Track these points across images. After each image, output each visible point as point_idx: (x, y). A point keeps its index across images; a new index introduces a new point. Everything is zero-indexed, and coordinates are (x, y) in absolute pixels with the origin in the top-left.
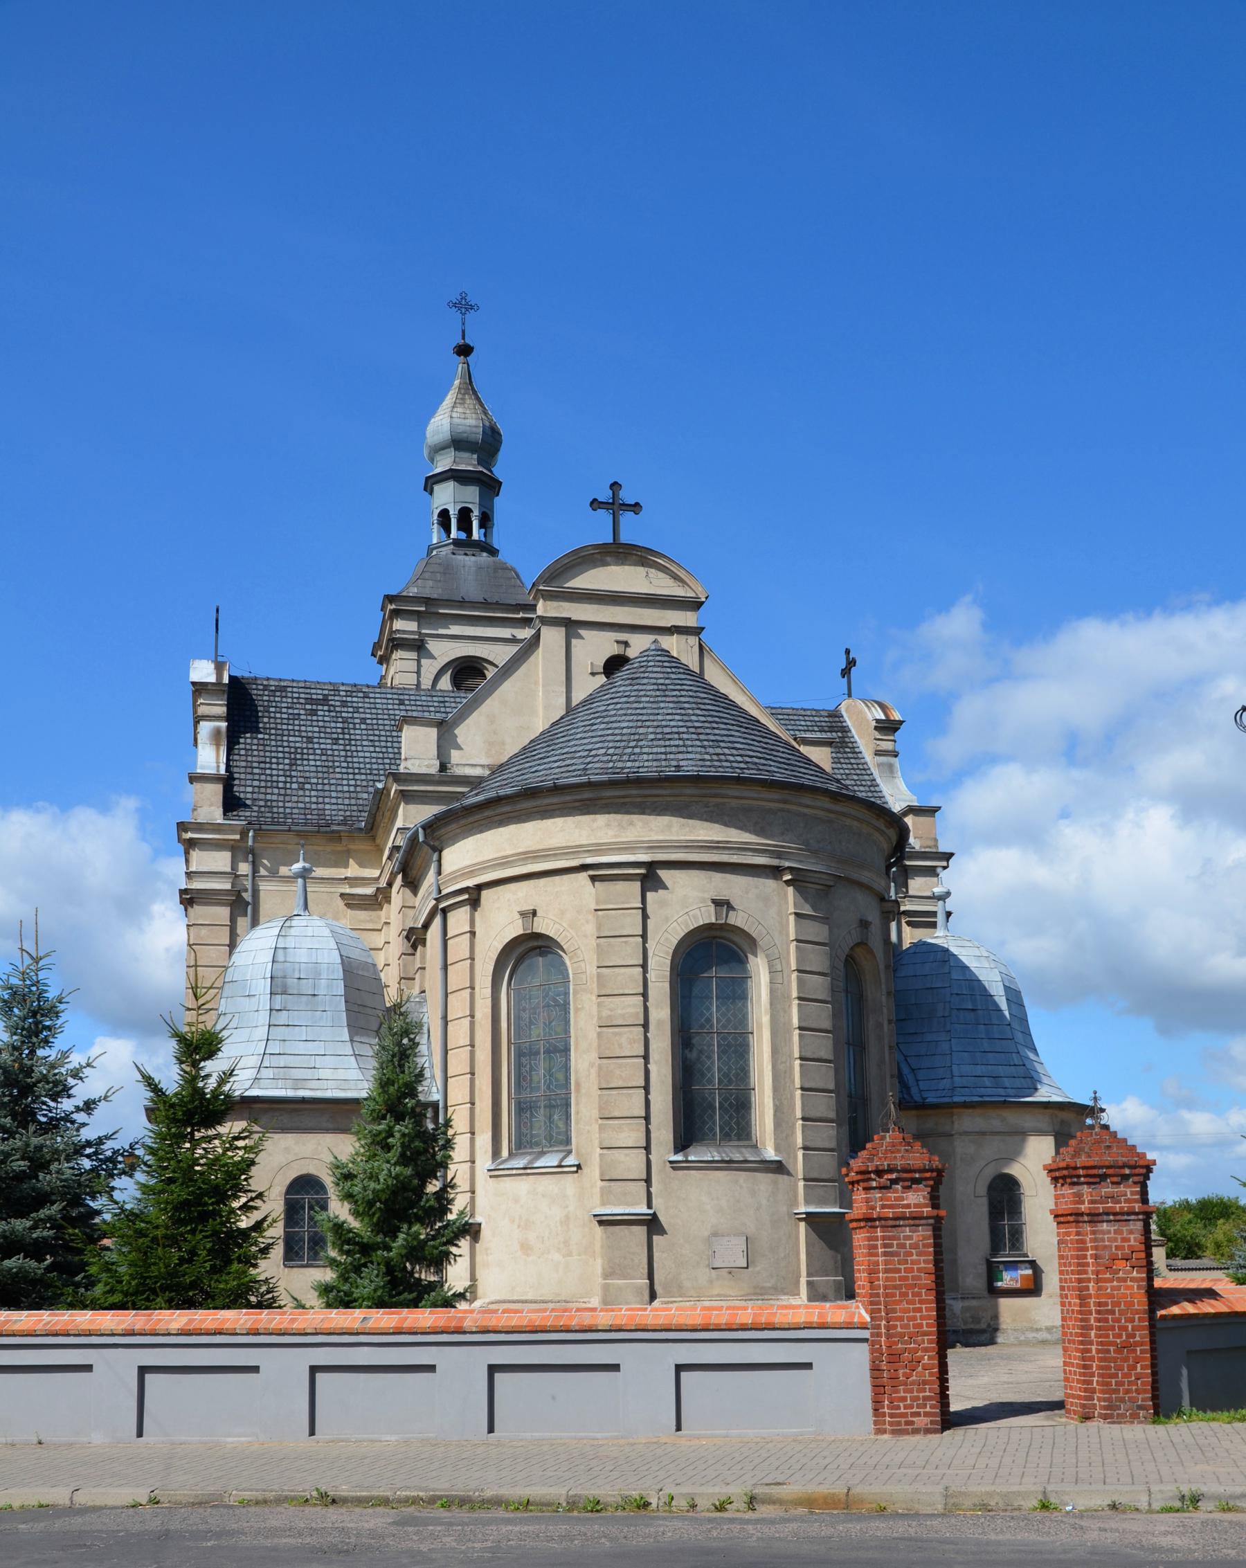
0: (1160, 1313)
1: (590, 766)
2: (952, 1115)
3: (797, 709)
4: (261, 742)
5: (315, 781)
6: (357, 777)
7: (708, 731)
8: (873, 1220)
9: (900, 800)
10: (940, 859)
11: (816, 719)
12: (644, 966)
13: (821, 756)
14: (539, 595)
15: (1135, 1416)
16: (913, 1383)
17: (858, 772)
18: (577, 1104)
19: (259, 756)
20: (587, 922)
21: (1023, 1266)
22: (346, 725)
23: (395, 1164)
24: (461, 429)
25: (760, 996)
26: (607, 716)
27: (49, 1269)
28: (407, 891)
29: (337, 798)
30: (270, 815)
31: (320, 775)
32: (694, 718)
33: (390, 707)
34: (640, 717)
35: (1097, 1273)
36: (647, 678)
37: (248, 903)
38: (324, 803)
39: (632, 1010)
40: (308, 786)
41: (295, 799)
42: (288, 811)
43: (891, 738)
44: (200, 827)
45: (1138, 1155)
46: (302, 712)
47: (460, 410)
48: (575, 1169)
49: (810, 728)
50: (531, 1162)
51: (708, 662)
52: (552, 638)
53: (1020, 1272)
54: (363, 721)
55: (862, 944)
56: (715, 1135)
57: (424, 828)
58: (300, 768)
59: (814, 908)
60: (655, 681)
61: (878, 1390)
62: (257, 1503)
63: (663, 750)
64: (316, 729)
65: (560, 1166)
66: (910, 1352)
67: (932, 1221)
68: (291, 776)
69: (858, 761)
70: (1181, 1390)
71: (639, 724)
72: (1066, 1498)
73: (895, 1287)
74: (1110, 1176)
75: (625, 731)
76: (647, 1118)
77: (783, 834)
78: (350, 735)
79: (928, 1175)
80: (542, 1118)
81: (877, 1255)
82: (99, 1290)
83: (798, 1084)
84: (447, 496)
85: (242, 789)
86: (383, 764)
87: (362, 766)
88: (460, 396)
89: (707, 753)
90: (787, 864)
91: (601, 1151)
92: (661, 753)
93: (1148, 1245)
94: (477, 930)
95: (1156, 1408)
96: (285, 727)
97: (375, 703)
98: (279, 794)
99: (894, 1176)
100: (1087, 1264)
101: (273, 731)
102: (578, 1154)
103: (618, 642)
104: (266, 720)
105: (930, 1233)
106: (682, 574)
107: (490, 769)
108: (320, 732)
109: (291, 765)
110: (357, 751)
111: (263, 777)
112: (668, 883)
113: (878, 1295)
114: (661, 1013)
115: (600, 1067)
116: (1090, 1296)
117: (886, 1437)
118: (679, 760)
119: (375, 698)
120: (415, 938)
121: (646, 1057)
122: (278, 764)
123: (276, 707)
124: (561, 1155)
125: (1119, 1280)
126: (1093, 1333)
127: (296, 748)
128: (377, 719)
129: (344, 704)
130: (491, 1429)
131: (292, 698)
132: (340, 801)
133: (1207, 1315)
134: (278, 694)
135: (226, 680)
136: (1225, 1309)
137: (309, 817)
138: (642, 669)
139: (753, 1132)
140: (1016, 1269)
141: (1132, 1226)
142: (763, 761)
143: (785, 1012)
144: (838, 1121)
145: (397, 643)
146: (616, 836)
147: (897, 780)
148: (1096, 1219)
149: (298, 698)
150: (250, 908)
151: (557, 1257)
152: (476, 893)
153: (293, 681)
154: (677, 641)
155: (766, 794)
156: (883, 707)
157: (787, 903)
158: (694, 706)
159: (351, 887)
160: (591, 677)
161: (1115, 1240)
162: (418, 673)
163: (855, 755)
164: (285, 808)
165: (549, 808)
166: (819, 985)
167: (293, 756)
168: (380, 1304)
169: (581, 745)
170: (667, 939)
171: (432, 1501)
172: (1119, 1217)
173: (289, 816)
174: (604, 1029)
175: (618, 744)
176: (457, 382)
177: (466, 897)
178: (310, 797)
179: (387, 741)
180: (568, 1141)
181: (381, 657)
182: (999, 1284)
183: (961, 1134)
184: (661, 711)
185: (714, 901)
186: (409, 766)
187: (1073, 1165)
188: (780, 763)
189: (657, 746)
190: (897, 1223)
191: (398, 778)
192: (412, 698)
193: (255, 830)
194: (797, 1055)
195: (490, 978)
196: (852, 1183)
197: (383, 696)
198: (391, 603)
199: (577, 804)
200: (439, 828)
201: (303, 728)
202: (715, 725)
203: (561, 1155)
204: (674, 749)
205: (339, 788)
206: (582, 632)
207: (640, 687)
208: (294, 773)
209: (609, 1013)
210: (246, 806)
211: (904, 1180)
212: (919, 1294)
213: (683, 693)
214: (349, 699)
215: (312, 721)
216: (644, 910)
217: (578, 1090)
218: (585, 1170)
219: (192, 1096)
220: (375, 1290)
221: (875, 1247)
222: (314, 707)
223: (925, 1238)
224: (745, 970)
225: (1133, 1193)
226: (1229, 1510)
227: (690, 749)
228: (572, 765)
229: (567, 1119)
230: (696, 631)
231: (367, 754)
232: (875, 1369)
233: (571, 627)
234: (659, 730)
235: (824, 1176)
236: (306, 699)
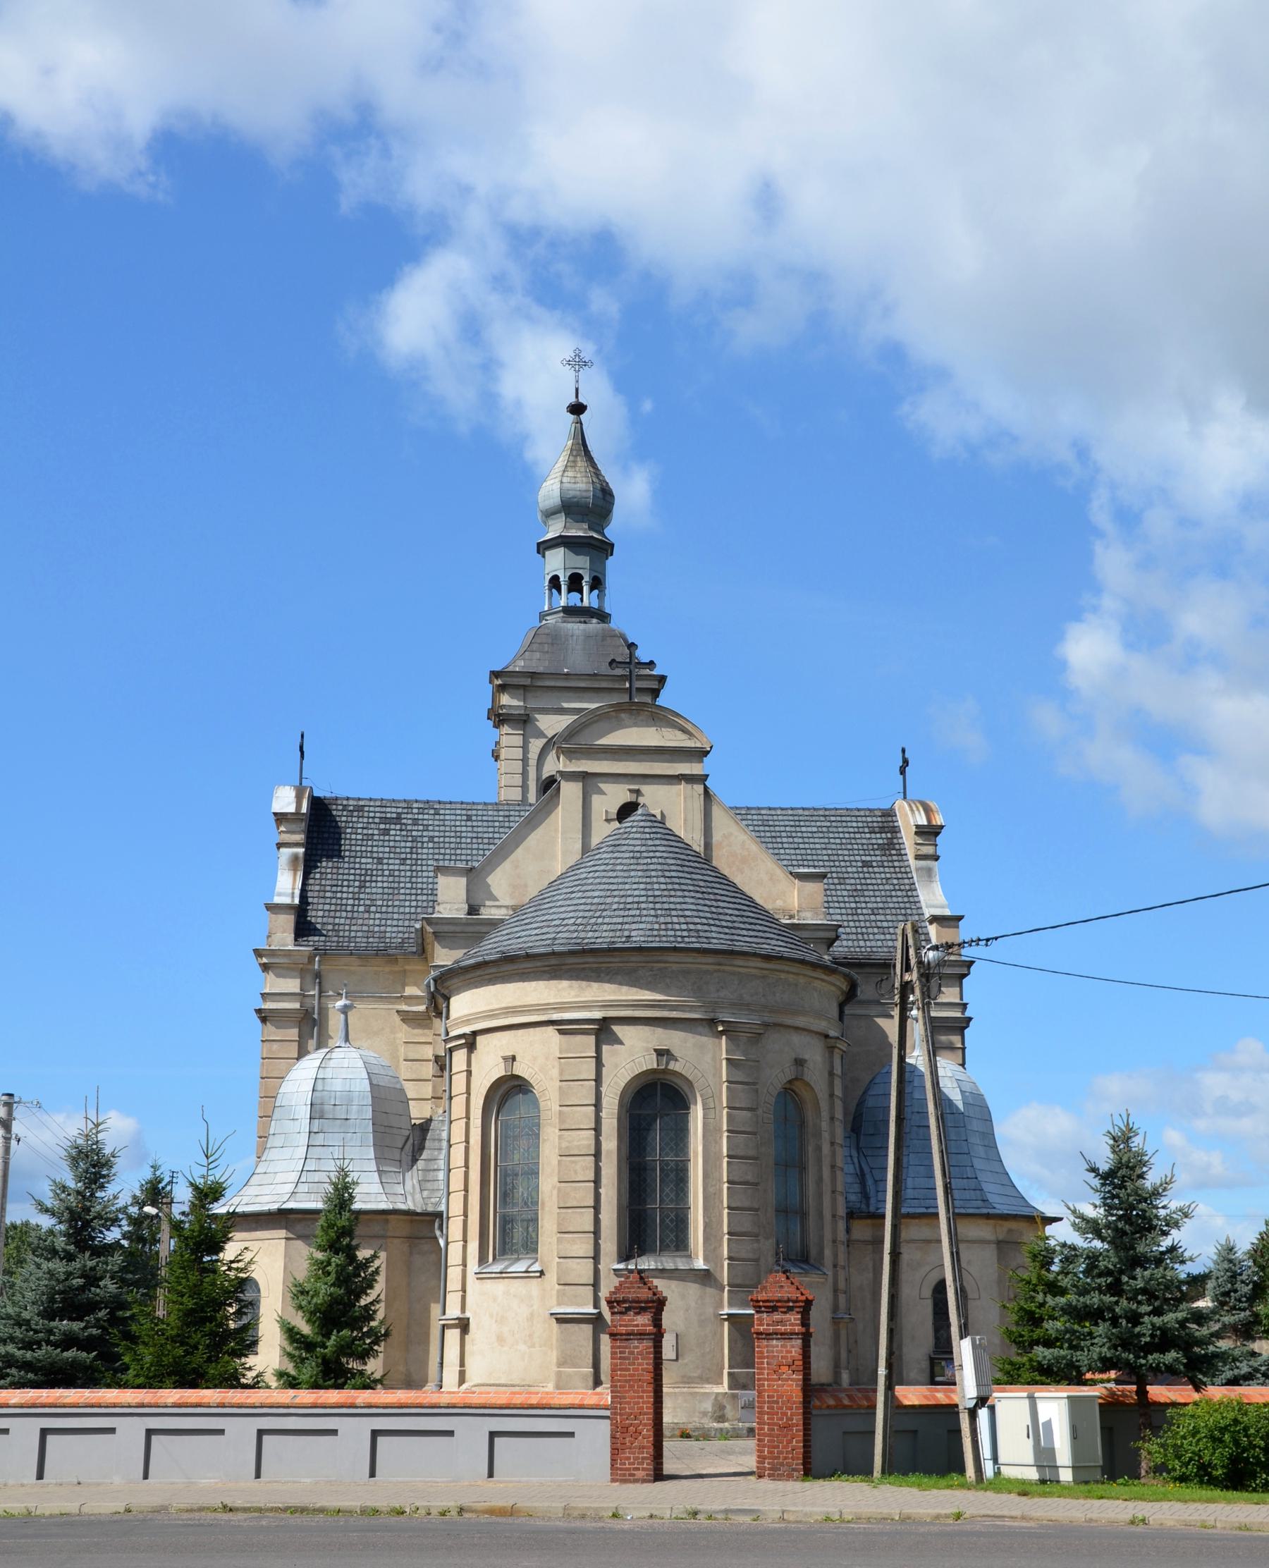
3: (851, 810)
5: (379, 903)
6: (419, 898)
7: (664, 899)
11: (869, 819)
16: (635, 1448)
17: (899, 875)
19: (332, 879)
22: (415, 844)
23: (332, 1285)
24: (572, 494)
26: (585, 884)
27: (95, 1358)
29: (398, 920)
30: (336, 939)
33: (458, 823)
39: (585, 1142)
40: (373, 909)
41: (360, 922)
42: (353, 934)
46: (376, 832)
48: (538, 1274)
50: (507, 1267)
52: (570, 792)
54: (431, 839)
58: (368, 890)
61: (615, 1452)
62: (187, 1511)
63: (620, 920)
64: (387, 849)
65: (526, 1272)
68: (359, 899)
69: (902, 864)
72: (627, 1511)
78: (417, 854)
82: (131, 1372)
84: (557, 562)
88: (572, 458)
94: (473, 1069)
102: (541, 1262)
106: (689, 727)
107: (514, 910)
108: (390, 853)
109: (360, 887)
110: (422, 871)
111: (334, 901)
112: (620, 1035)
118: (631, 930)
122: (348, 886)
123: (352, 828)
127: (366, 870)
131: (368, 817)
132: (401, 923)
134: (355, 814)
137: (371, 940)
138: (625, 836)
141: (794, 1342)
142: (706, 928)
143: (716, 1142)
146: (577, 996)
147: (934, 884)
151: (522, 1347)
153: (371, 800)
156: (928, 811)
160: (606, 823)
161: (782, 1352)
163: (900, 858)
164: (350, 931)
165: (526, 971)
167: (363, 878)
168: (315, 1386)
170: (616, 1083)
171: (285, 1510)
172: (785, 1336)
177: (463, 1041)
178: (374, 921)
180: (535, 1250)
185: (656, 1050)
186: (441, 910)
192: (480, 813)
197: (453, 812)
198: (497, 678)
200: (446, 980)
203: (530, 1262)
205: (402, 910)
208: (362, 896)
209: (567, 1144)
211: (635, 1308)
212: (642, 1387)
214: (421, 817)
215: (384, 841)
217: (543, 1209)
218: (548, 1275)
219: (200, 1233)
222: (388, 826)
225: (795, 1319)
230: (702, 779)
234: (623, 900)
236: (380, 818)
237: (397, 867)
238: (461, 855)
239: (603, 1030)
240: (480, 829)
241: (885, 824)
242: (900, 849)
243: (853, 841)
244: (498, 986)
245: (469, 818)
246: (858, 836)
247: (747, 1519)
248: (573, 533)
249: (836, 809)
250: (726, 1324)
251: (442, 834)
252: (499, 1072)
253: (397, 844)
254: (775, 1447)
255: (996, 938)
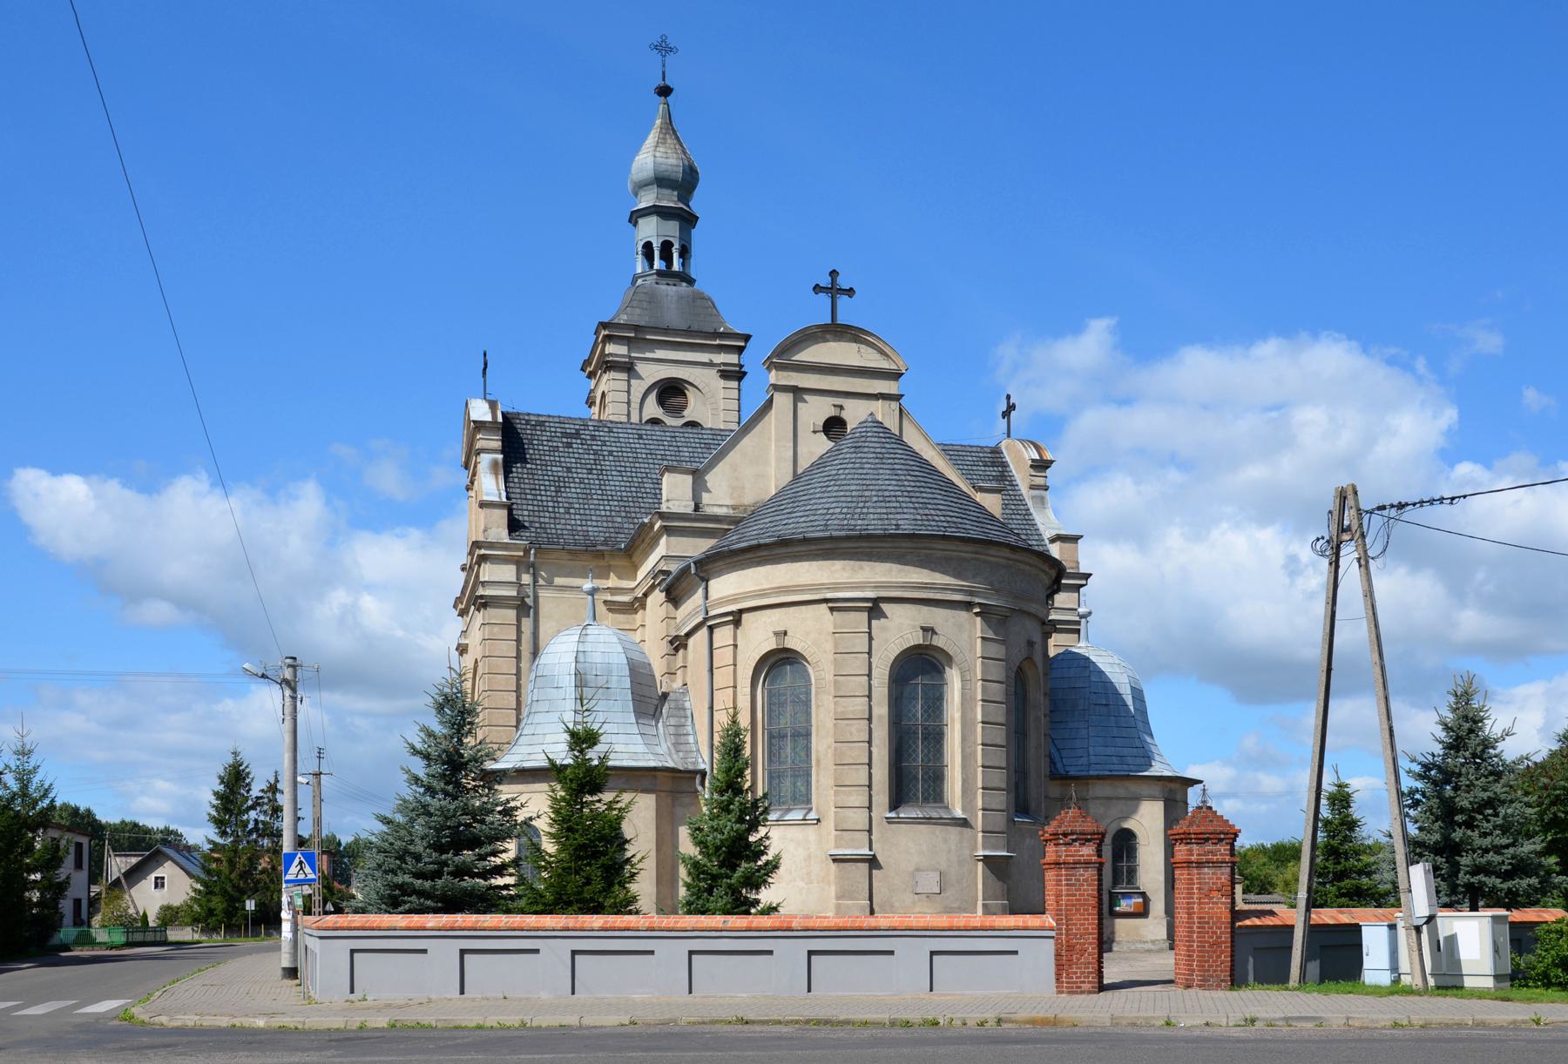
0: (1238, 924)
1: (830, 522)
2: (1088, 784)
3: (965, 446)
4: (530, 471)
6: (611, 503)
7: (918, 494)
8: (1060, 864)
9: (1049, 528)
10: (1081, 579)
11: (981, 455)
12: (869, 675)
13: (992, 503)
14: (772, 366)
15: (1219, 986)
16: (1081, 963)
17: (1015, 502)
18: (818, 775)
19: (530, 484)
20: (827, 641)
21: (1136, 896)
24: (663, 168)
25: (953, 698)
28: (670, 606)
29: (597, 521)
31: (581, 501)
32: (906, 483)
33: (631, 441)
34: (864, 482)
35: (1200, 899)
36: (868, 447)
37: (531, 607)
38: (587, 525)
39: (859, 708)
40: (572, 511)
41: (563, 521)
42: (559, 532)
43: (1043, 474)
44: (491, 545)
45: (1230, 826)
46: (560, 445)
47: (662, 149)
49: (976, 463)
50: (782, 816)
51: (906, 423)
53: (1133, 900)
54: (610, 453)
55: (1029, 658)
56: (918, 798)
57: (695, 563)
58: (564, 495)
59: (996, 634)
60: (874, 450)
61: (1060, 967)
62: (699, 1023)
63: (884, 511)
64: (573, 460)
66: (1081, 944)
67: (1097, 865)
68: (557, 502)
69: (1015, 493)
70: (1247, 970)
71: (865, 488)
72: (1181, 1020)
73: (1073, 905)
74: (1211, 839)
75: (854, 494)
76: (870, 786)
77: (974, 577)
79: (1096, 836)
80: (788, 784)
81: (1061, 885)
83: (980, 762)
84: (650, 230)
85: (520, 512)
86: (631, 492)
87: (614, 493)
89: (918, 514)
90: (977, 600)
91: (836, 810)
92: (884, 513)
93: (1233, 883)
95: (1232, 981)
96: (547, 458)
97: (619, 437)
98: (550, 518)
99: (1074, 837)
100: (1194, 893)
101: (538, 462)
102: (818, 811)
103: (835, 406)
104: (531, 451)
105: (1096, 872)
106: (887, 350)
113: (1061, 910)
114: (881, 710)
115: (836, 749)
116: (1194, 913)
117: (1063, 995)
119: (618, 433)
120: (678, 643)
121: (870, 742)
122: (546, 491)
123: (538, 440)
124: (805, 812)
125: (1213, 903)
126: (1195, 935)
127: (559, 477)
128: (622, 452)
129: (593, 438)
130: (809, 991)
131: (551, 432)
132: (599, 524)
133: (1268, 926)
134: (538, 428)
135: (500, 419)
136: (1279, 923)
138: (863, 439)
139: (945, 797)
140: (1131, 898)
141: (1223, 870)
143: (972, 710)
144: (1007, 790)
145: (609, 365)
146: (849, 578)
148: (1201, 865)
149: (555, 432)
150: (532, 610)
151: (801, 884)
152: (738, 615)
153: (549, 416)
154: (882, 406)
155: (963, 547)
157: (976, 629)
158: (905, 472)
159: (612, 595)
161: (1212, 879)
162: (628, 392)
164: (556, 529)
166: (997, 691)
167: (557, 484)
169: (820, 504)
172: (1216, 864)
173: (560, 536)
174: (839, 721)
175: (850, 505)
176: (658, 122)
179: (632, 472)
180: (809, 801)
181: (590, 372)
182: (1118, 909)
183: (1093, 799)
184: (881, 477)
185: (922, 628)
186: (671, 506)
187: (1188, 832)
188: (973, 521)
189: (880, 508)
190: (1075, 866)
191: (662, 516)
192: (649, 432)
193: (536, 549)
194: (980, 742)
195: (750, 680)
196: (1046, 841)
197: (625, 431)
198: (605, 329)
199: (820, 552)
200: (707, 563)
201: (562, 459)
202: (922, 489)
204: (893, 510)
205: (598, 513)
206: (806, 397)
207: (863, 455)
208: (559, 499)
210: (525, 527)
211: (1082, 839)
212: (1088, 910)
213: (897, 461)
214: (597, 433)
215: (569, 453)
216: (870, 633)
218: (823, 823)
220: (725, 904)
221: (1061, 880)
222: (569, 440)
223: (1093, 875)
224: (943, 679)
226: (1272, 1026)
227: (905, 510)
228: (816, 520)
229: (808, 785)
231: (617, 483)
232: (1058, 955)
233: (798, 392)
234: (880, 493)
235: (997, 830)
236: (561, 433)
237: (585, 476)
238: (640, 468)
239: (874, 609)
240: (652, 447)
241: (995, 460)
242: (1012, 481)
243: (972, 472)
244: (768, 568)
245: (640, 437)
246: (975, 468)
247: (1310, 1025)
248: (664, 203)
249: (953, 445)
250: (980, 864)
251: (619, 449)
252: (771, 645)
253: (581, 456)
254: (1205, 962)
255: (1465, 497)
